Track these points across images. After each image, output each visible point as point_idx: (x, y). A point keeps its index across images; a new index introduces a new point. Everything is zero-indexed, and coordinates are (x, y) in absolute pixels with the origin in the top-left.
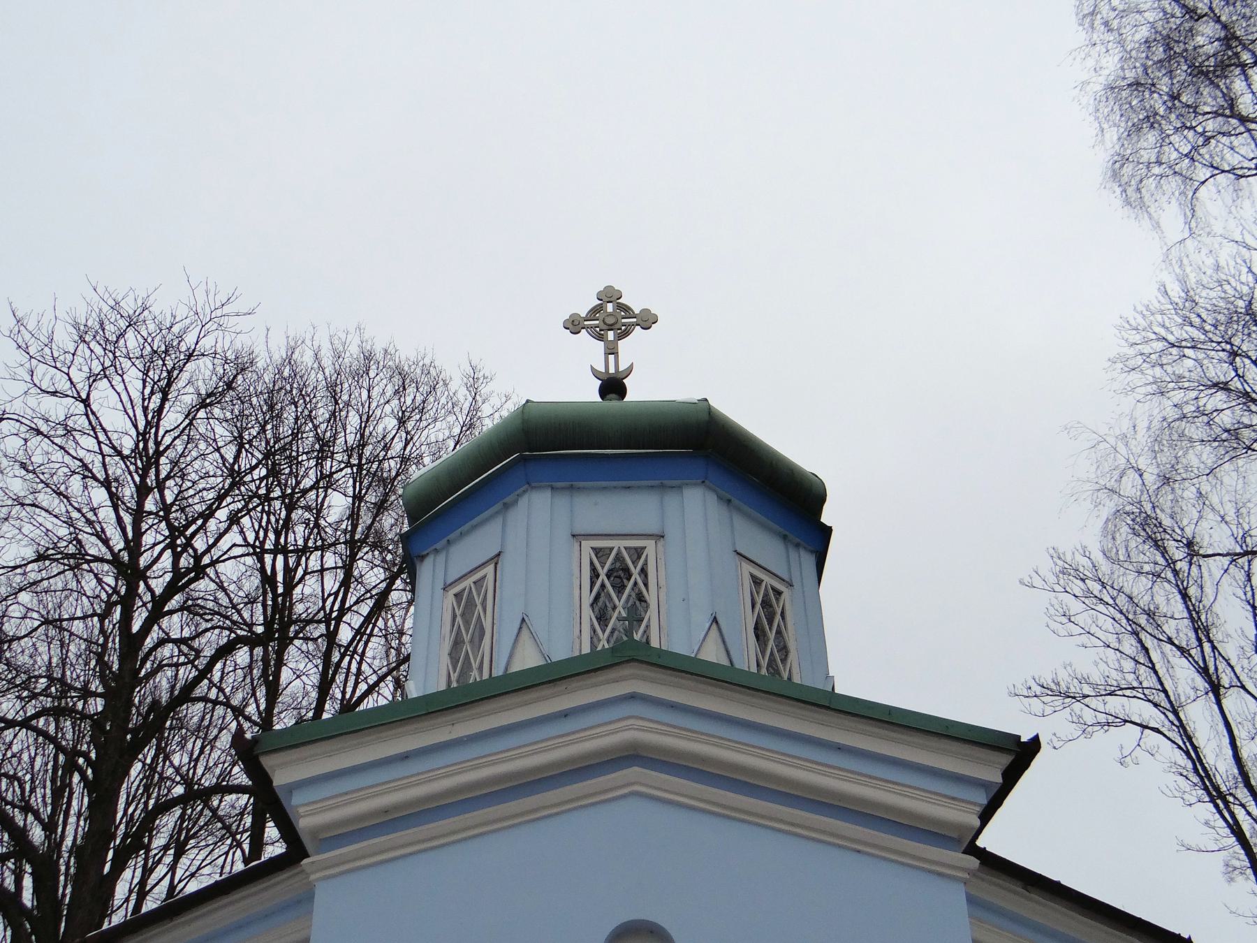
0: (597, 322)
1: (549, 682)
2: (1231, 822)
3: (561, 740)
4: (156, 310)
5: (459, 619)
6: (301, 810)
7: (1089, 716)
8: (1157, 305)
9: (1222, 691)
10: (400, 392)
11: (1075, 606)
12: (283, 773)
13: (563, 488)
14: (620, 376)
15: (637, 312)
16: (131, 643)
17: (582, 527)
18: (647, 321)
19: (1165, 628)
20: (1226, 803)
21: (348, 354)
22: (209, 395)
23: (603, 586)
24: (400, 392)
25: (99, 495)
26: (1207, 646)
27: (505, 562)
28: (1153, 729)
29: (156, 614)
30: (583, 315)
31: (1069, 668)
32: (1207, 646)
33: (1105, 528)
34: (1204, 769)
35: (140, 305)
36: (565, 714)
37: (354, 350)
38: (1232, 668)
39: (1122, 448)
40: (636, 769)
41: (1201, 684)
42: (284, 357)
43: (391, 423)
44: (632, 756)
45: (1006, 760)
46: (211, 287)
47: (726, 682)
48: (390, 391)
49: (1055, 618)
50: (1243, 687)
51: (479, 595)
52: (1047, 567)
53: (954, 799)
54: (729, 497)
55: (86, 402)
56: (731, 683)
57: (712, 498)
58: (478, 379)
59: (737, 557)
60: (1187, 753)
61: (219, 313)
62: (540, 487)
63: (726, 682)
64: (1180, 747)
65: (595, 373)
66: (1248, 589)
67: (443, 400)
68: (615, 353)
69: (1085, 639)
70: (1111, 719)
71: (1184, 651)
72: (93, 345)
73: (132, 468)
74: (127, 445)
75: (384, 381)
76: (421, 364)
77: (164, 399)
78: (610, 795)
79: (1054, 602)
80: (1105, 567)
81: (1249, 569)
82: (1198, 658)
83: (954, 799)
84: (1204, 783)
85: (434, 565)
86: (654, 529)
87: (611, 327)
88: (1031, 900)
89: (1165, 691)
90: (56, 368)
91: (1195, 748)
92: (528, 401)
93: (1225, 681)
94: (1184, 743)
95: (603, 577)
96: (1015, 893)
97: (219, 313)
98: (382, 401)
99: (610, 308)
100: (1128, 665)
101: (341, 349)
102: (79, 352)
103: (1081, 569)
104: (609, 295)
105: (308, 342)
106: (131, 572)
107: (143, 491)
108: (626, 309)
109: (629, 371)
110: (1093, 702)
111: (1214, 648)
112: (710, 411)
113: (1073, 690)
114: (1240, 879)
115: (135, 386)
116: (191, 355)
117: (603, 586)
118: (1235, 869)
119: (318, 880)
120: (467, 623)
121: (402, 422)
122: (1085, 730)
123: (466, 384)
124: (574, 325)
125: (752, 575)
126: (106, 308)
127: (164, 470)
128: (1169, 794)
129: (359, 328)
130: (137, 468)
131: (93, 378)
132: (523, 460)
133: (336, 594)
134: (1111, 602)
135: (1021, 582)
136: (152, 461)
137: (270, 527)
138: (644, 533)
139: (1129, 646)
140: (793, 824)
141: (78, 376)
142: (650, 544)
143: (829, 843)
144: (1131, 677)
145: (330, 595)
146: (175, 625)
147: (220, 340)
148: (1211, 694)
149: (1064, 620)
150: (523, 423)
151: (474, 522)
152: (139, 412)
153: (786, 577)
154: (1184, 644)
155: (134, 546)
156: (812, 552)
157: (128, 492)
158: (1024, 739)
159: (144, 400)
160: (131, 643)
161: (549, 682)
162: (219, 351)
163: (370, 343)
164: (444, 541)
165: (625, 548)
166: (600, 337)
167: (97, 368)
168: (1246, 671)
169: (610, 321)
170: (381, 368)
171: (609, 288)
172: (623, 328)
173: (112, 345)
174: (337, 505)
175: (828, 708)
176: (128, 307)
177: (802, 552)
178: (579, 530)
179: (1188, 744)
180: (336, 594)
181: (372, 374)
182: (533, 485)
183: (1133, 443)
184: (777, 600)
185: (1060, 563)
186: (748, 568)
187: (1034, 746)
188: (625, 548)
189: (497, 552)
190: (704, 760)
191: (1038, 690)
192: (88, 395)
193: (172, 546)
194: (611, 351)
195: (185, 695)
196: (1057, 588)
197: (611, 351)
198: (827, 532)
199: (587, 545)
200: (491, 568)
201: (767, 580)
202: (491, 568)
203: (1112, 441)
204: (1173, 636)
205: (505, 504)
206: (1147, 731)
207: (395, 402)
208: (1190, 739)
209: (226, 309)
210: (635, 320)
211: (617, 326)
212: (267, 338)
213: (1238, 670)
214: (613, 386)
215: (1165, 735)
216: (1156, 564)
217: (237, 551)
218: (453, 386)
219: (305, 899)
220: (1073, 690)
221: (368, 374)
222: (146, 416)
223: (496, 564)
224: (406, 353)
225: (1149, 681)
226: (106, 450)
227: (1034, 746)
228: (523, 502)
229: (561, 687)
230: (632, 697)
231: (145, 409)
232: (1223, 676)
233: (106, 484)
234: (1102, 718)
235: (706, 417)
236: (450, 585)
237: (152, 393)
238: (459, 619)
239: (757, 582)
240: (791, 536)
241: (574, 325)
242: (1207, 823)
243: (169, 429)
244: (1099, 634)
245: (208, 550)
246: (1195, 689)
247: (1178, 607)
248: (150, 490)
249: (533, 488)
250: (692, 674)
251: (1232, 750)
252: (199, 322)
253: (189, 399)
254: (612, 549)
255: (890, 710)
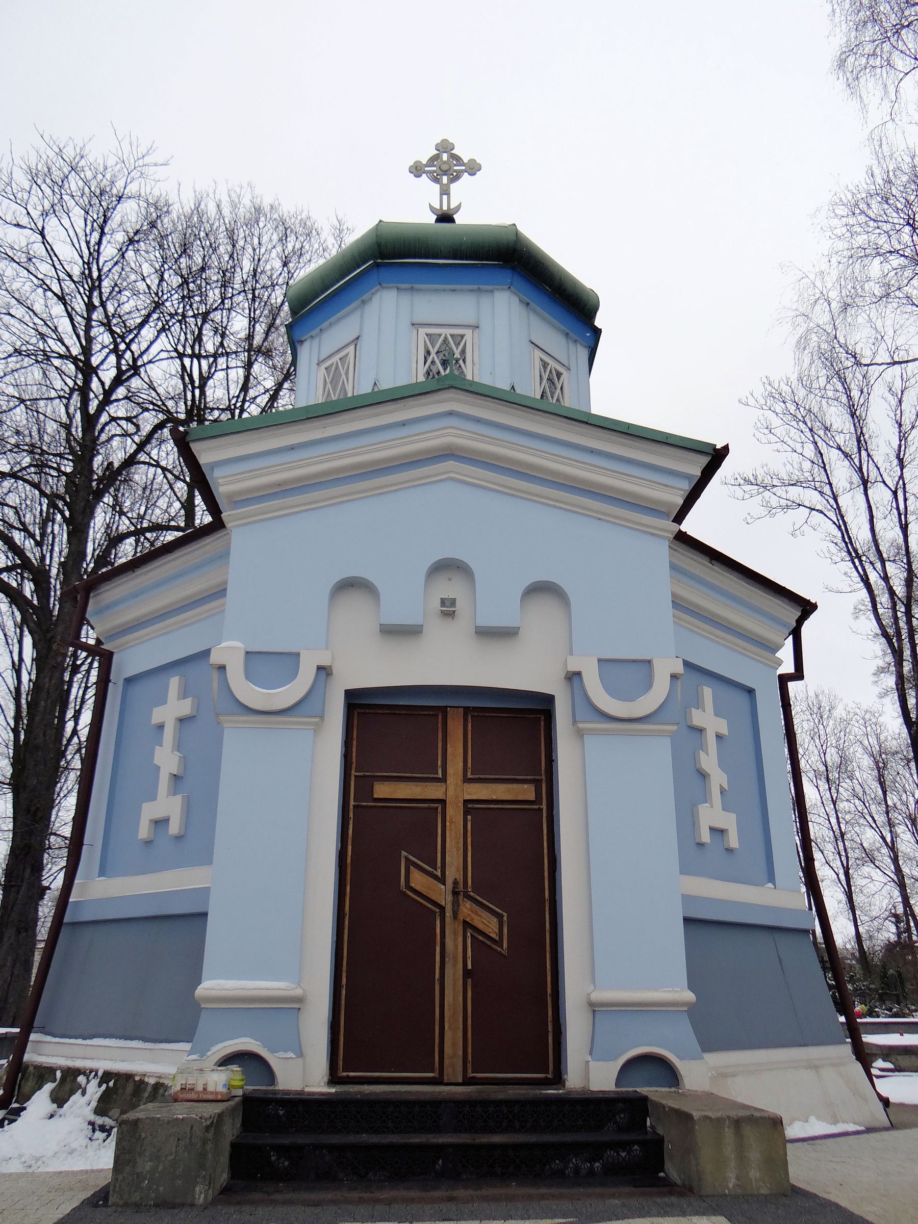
0: (435, 168)
1: (393, 400)
2: (862, 573)
3: (399, 441)
4: (91, 158)
5: (329, 385)
6: (220, 481)
7: (774, 501)
8: (865, 186)
9: (869, 485)
10: (283, 239)
11: (776, 422)
12: (205, 454)
13: (405, 289)
14: (450, 212)
15: (466, 161)
16: (89, 421)
17: (420, 318)
18: (473, 168)
19: (837, 438)
20: (861, 561)
21: (242, 205)
22: (136, 233)
23: (433, 362)
24: (283, 239)
25: (58, 309)
26: (864, 453)
27: (364, 344)
28: (817, 510)
29: (107, 401)
30: (424, 162)
31: (765, 467)
32: (864, 453)
33: (798, 342)
34: (849, 538)
35: (78, 152)
36: (403, 424)
37: (246, 201)
38: (878, 469)
39: (818, 284)
40: (452, 462)
41: (856, 479)
42: (193, 207)
43: (278, 264)
44: (449, 454)
45: (705, 460)
46: (134, 140)
47: (516, 404)
48: (275, 237)
49: (761, 430)
50: (884, 482)
51: (343, 368)
52: (759, 391)
53: (666, 486)
54: (528, 301)
55: (42, 234)
56: (520, 405)
57: (515, 300)
58: (343, 230)
59: (531, 345)
60: (839, 527)
61: (141, 162)
62: (389, 288)
63: (516, 404)
64: (834, 523)
65: (432, 209)
66: (898, 412)
67: (316, 246)
68: (448, 194)
69: (779, 446)
70: (789, 503)
71: (846, 455)
72: (44, 186)
73: (82, 290)
74: (76, 271)
75: (271, 231)
76: (299, 218)
77: (102, 234)
78: (434, 479)
79: (761, 418)
80: (801, 393)
81: (901, 397)
82: (857, 461)
83: (666, 486)
84: (847, 547)
85: (310, 351)
86: (472, 321)
87: (445, 173)
88: (713, 570)
89: (830, 484)
90: (17, 203)
91: (845, 523)
92: (380, 221)
93: (872, 479)
94: (838, 520)
95: (433, 355)
96: (704, 565)
97: (141, 162)
98: (270, 247)
99: (445, 157)
100: (807, 465)
101: (237, 201)
102: (33, 192)
103: (784, 394)
104: (445, 147)
105: (211, 195)
106: (88, 370)
107: (90, 307)
108: (457, 158)
109: (458, 208)
110: (779, 491)
111: (869, 455)
112: (517, 233)
113: (766, 481)
114: (862, 618)
115: (79, 223)
116: (120, 198)
117: (433, 362)
118: (861, 610)
119: (234, 527)
120: (334, 389)
121: (285, 264)
122: (771, 510)
123: (334, 234)
124: (417, 170)
125: (541, 360)
126: (52, 154)
127: (106, 290)
128: (822, 555)
129: (249, 184)
130: (84, 289)
131: (44, 214)
132: (377, 265)
133: (238, 397)
134: (802, 419)
135: (740, 401)
136: (96, 286)
137: (188, 344)
138: (464, 324)
139: (810, 450)
140: (557, 501)
141: (35, 214)
142: (468, 333)
143: (581, 514)
144: (807, 474)
145: (233, 397)
146: (118, 410)
147: (143, 185)
148: (862, 486)
149: (767, 431)
150: (377, 238)
151: (338, 315)
152: (84, 245)
153: (566, 364)
154: (848, 450)
155: (87, 351)
156: (586, 347)
157: (79, 305)
158: (718, 447)
159: (86, 235)
160: (89, 421)
161: (393, 400)
162: (143, 194)
163: (259, 198)
164: (317, 330)
165: (452, 336)
166: (436, 180)
167: (47, 205)
168: (888, 471)
169: (445, 167)
170: (268, 219)
171: (445, 141)
172: (455, 174)
173: (60, 185)
174: (239, 325)
175: (587, 423)
176: (69, 153)
177: (579, 346)
178: (418, 319)
179: (841, 521)
180: (238, 397)
181: (261, 224)
182: (384, 285)
183: (827, 278)
184: (559, 379)
185: (769, 388)
186: (538, 354)
187: (726, 450)
188: (451, 335)
189: (357, 336)
190: (498, 457)
191: (742, 482)
192: (43, 228)
193: (115, 351)
194: (445, 191)
195: (130, 461)
196: (764, 407)
197: (445, 191)
198: (597, 332)
199: (423, 331)
200: (352, 348)
201: (552, 364)
202: (352, 348)
203: (812, 277)
204: (842, 444)
205: (363, 301)
206: (814, 512)
207: (279, 248)
208: (842, 517)
209: (147, 160)
210: (463, 168)
211: (450, 172)
212: (179, 191)
213: (882, 470)
214: (445, 218)
215: (825, 515)
216: (837, 391)
217: (164, 355)
218: (323, 236)
219: (225, 555)
220: (766, 481)
221: (258, 224)
222: (89, 248)
223: (356, 345)
224: (287, 208)
225: (821, 476)
226: (62, 276)
227: (726, 450)
228: (376, 299)
229: (401, 404)
230: (451, 414)
231: (88, 243)
232: (871, 474)
233: (62, 298)
234: (783, 502)
235: (513, 238)
236: (322, 361)
237: (93, 230)
238: (329, 385)
239: (545, 365)
240: (571, 334)
241: (417, 170)
242: (845, 574)
243: (107, 259)
244: (790, 442)
245: (142, 354)
246: (851, 483)
247: (848, 426)
248: (95, 307)
249: (383, 288)
250: (493, 398)
251: (900, 702)
252: (125, 170)
253: (120, 237)
254: (440, 335)
255: (629, 425)
